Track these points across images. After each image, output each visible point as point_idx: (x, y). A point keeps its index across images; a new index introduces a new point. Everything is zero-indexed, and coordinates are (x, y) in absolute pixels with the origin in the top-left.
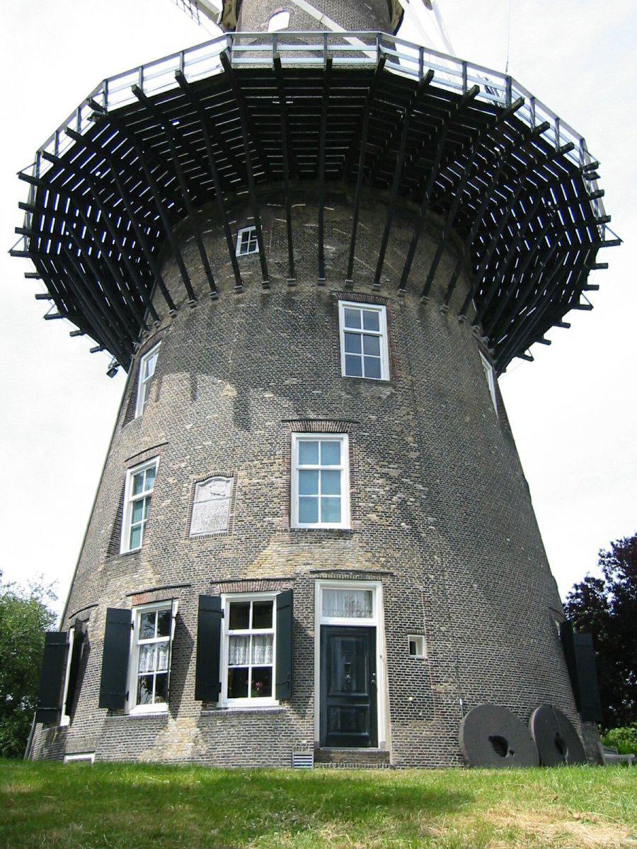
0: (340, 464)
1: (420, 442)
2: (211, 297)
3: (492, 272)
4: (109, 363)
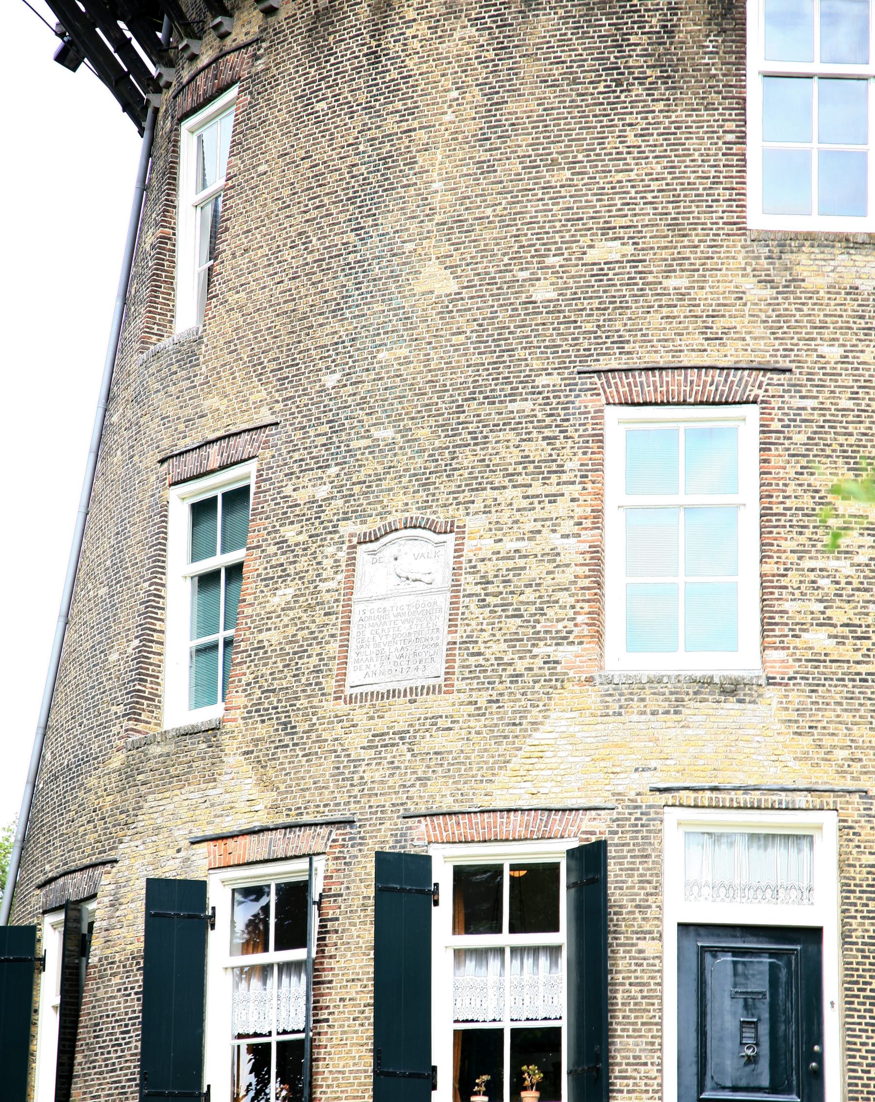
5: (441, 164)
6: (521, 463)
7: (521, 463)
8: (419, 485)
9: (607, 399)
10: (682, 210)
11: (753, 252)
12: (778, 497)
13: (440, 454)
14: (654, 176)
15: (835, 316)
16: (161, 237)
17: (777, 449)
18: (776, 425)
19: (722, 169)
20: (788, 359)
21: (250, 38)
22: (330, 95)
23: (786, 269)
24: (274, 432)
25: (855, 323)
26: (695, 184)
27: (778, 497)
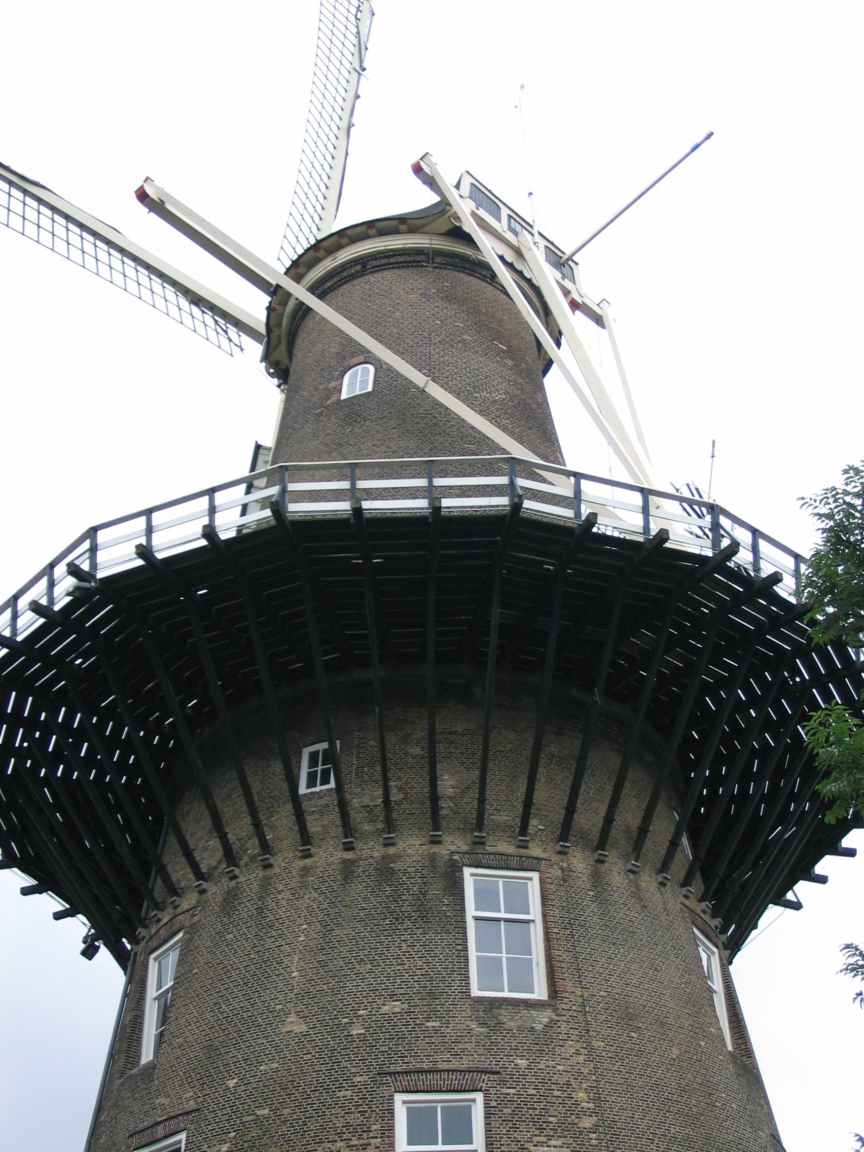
0: (472, 1143)
1: (597, 1099)
2: (262, 863)
3: (714, 781)
4: (84, 935)
5: (298, 962)
6: (345, 1126)
7: (345, 1126)
8: (284, 1141)
9: (395, 1089)
10: (434, 985)
11: (475, 1008)
12: (496, 1145)
13: (296, 1123)
14: (418, 967)
15: (523, 1043)
16: (135, 1016)
17: (495, 1117)
18: (493, 1104)
19: (455, 963)
20: (498, 1066)
21: (191, 906)
22: (235, 931)
23: (494, 1017)
24: (197, 1114)
25: (534, 1047)
26: (441, 971)
27: (496, 1145)
